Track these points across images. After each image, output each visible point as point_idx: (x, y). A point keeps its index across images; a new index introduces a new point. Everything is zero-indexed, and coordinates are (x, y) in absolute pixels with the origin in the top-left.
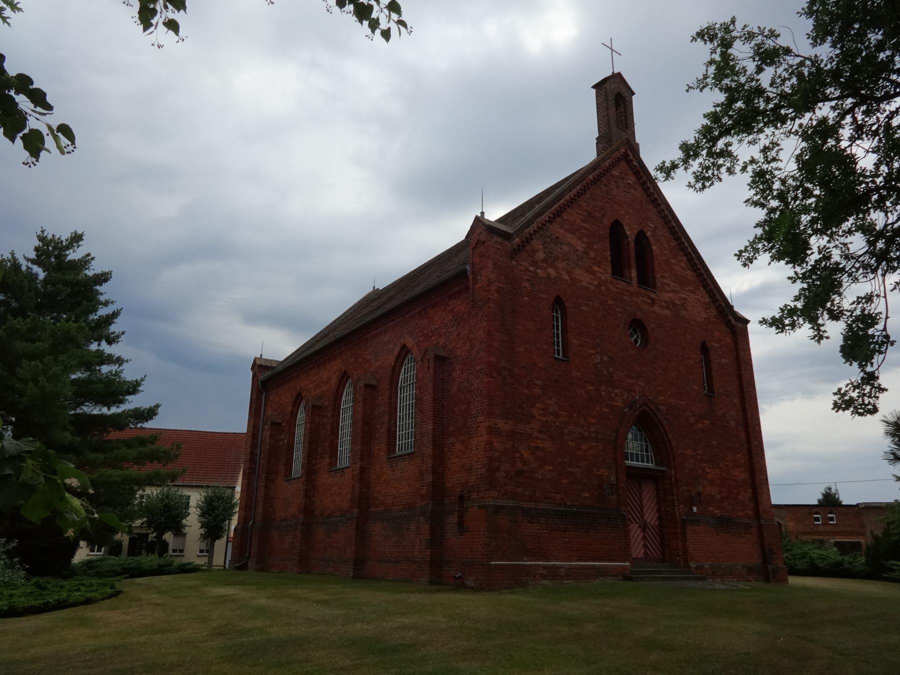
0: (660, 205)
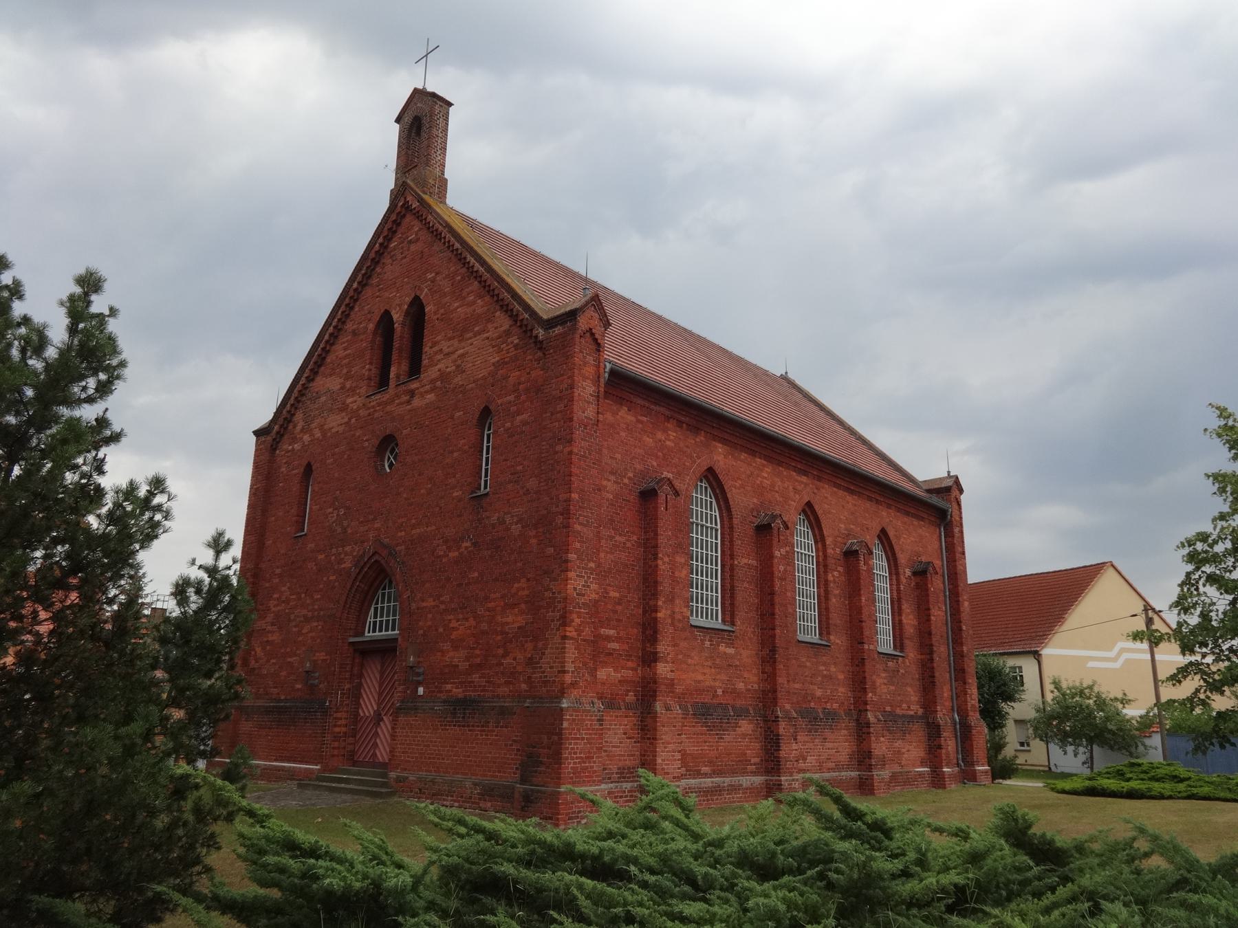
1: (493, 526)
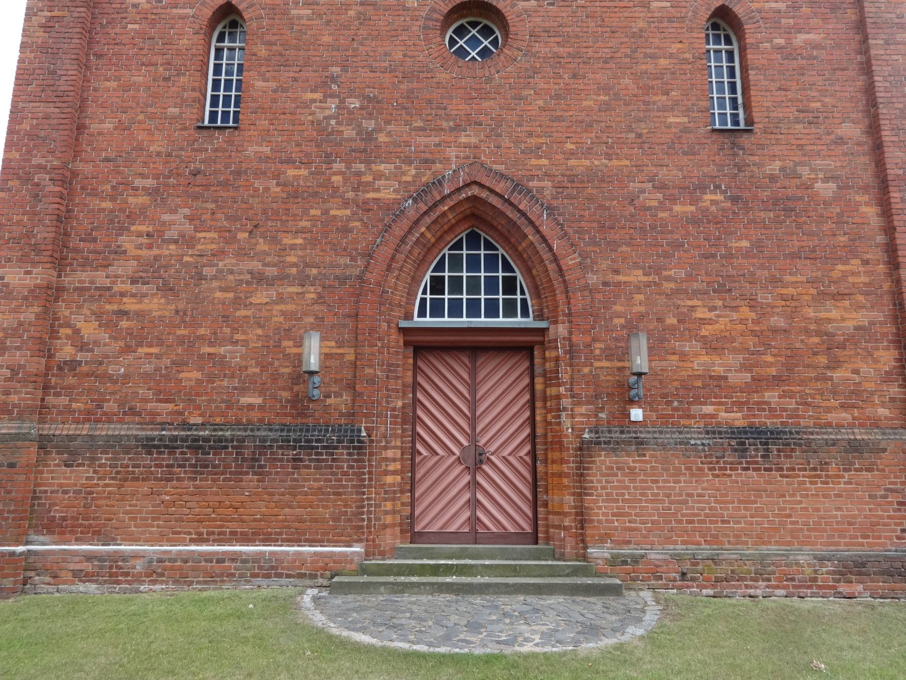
1: (773, 178)
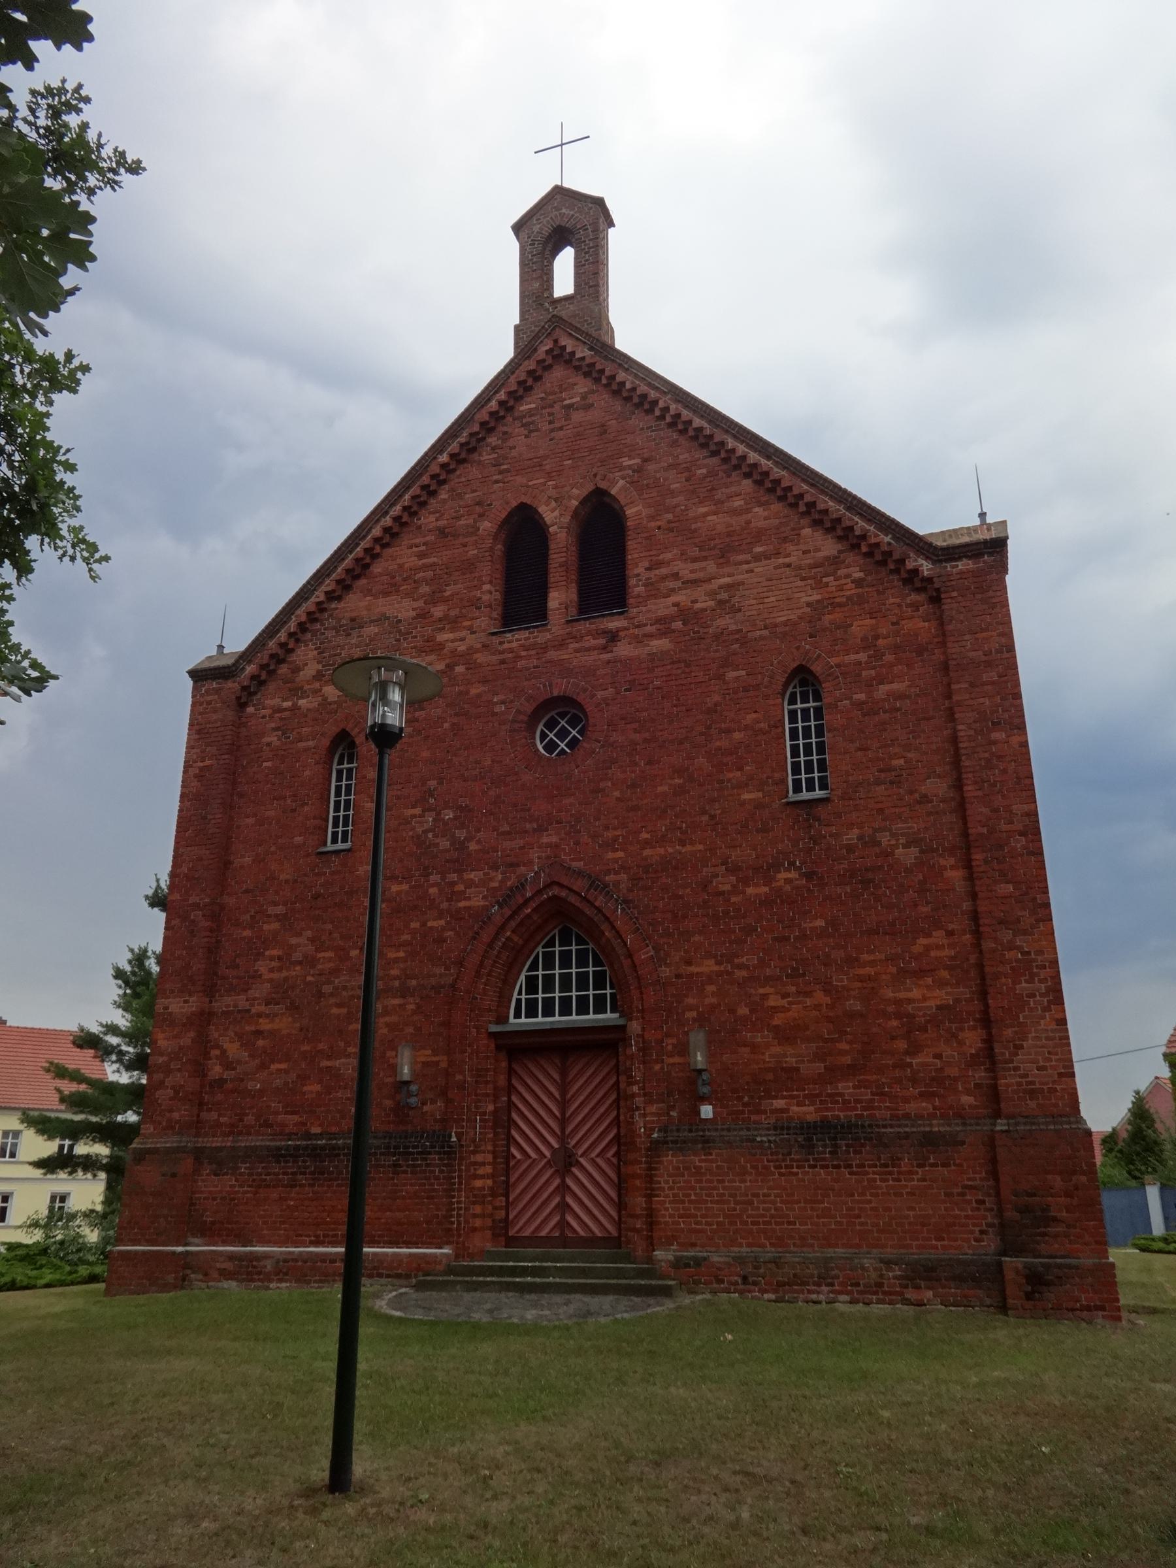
0: (655, 403)
1: (850, 848)
